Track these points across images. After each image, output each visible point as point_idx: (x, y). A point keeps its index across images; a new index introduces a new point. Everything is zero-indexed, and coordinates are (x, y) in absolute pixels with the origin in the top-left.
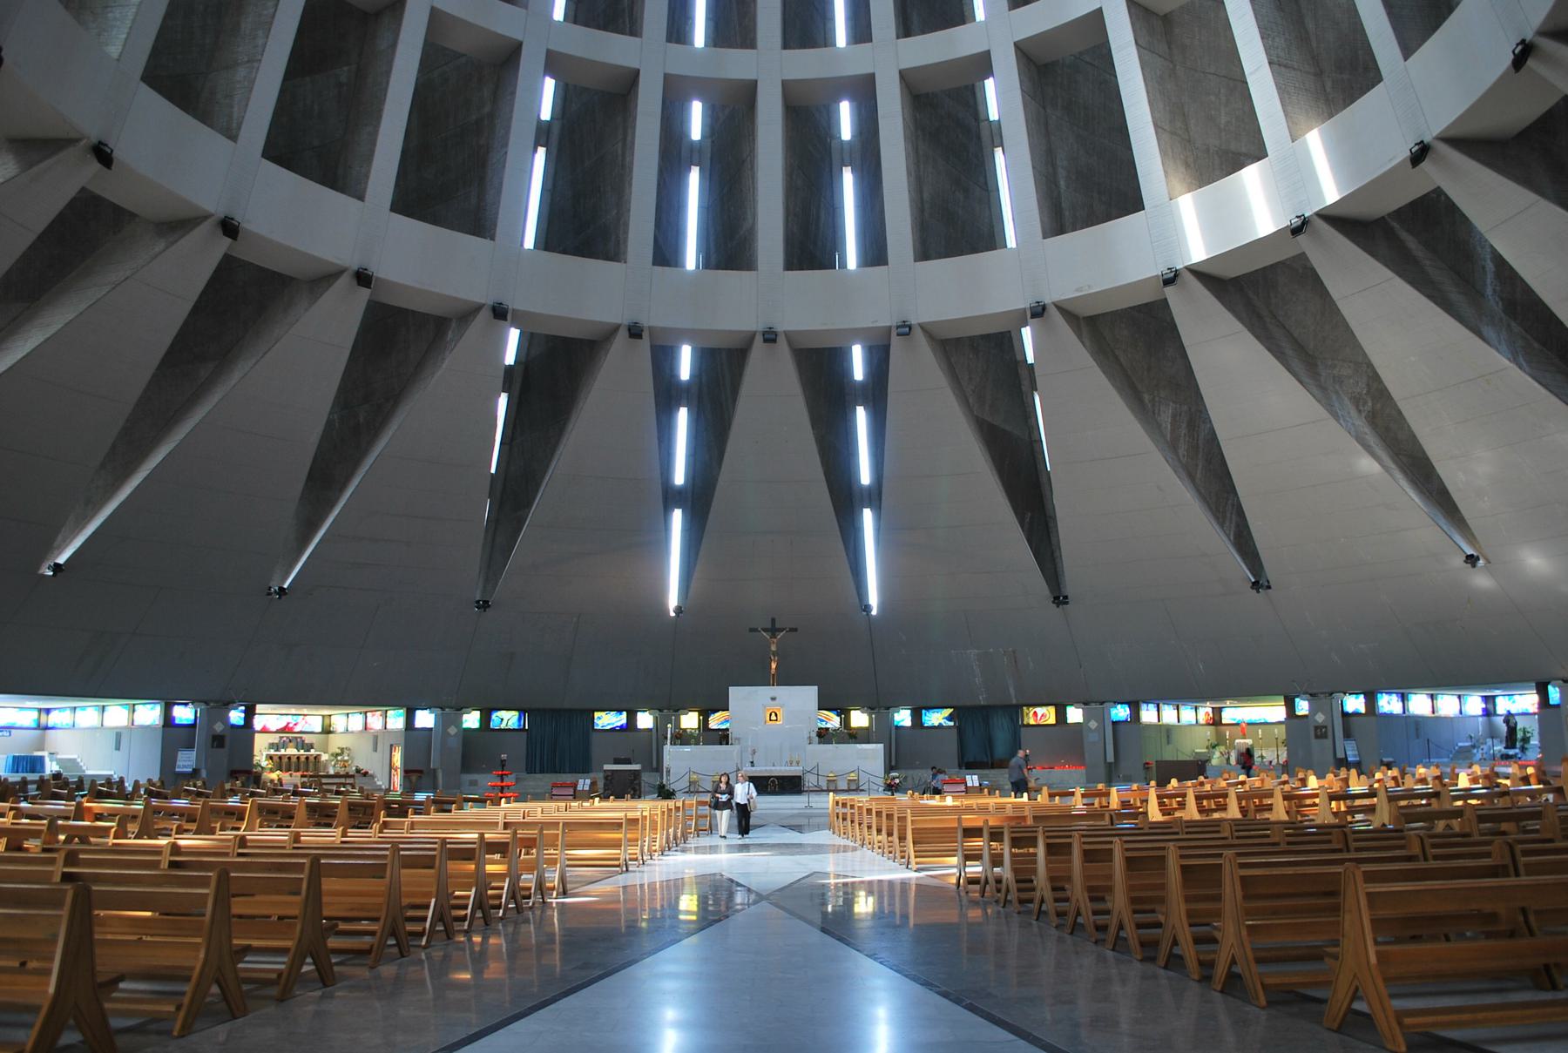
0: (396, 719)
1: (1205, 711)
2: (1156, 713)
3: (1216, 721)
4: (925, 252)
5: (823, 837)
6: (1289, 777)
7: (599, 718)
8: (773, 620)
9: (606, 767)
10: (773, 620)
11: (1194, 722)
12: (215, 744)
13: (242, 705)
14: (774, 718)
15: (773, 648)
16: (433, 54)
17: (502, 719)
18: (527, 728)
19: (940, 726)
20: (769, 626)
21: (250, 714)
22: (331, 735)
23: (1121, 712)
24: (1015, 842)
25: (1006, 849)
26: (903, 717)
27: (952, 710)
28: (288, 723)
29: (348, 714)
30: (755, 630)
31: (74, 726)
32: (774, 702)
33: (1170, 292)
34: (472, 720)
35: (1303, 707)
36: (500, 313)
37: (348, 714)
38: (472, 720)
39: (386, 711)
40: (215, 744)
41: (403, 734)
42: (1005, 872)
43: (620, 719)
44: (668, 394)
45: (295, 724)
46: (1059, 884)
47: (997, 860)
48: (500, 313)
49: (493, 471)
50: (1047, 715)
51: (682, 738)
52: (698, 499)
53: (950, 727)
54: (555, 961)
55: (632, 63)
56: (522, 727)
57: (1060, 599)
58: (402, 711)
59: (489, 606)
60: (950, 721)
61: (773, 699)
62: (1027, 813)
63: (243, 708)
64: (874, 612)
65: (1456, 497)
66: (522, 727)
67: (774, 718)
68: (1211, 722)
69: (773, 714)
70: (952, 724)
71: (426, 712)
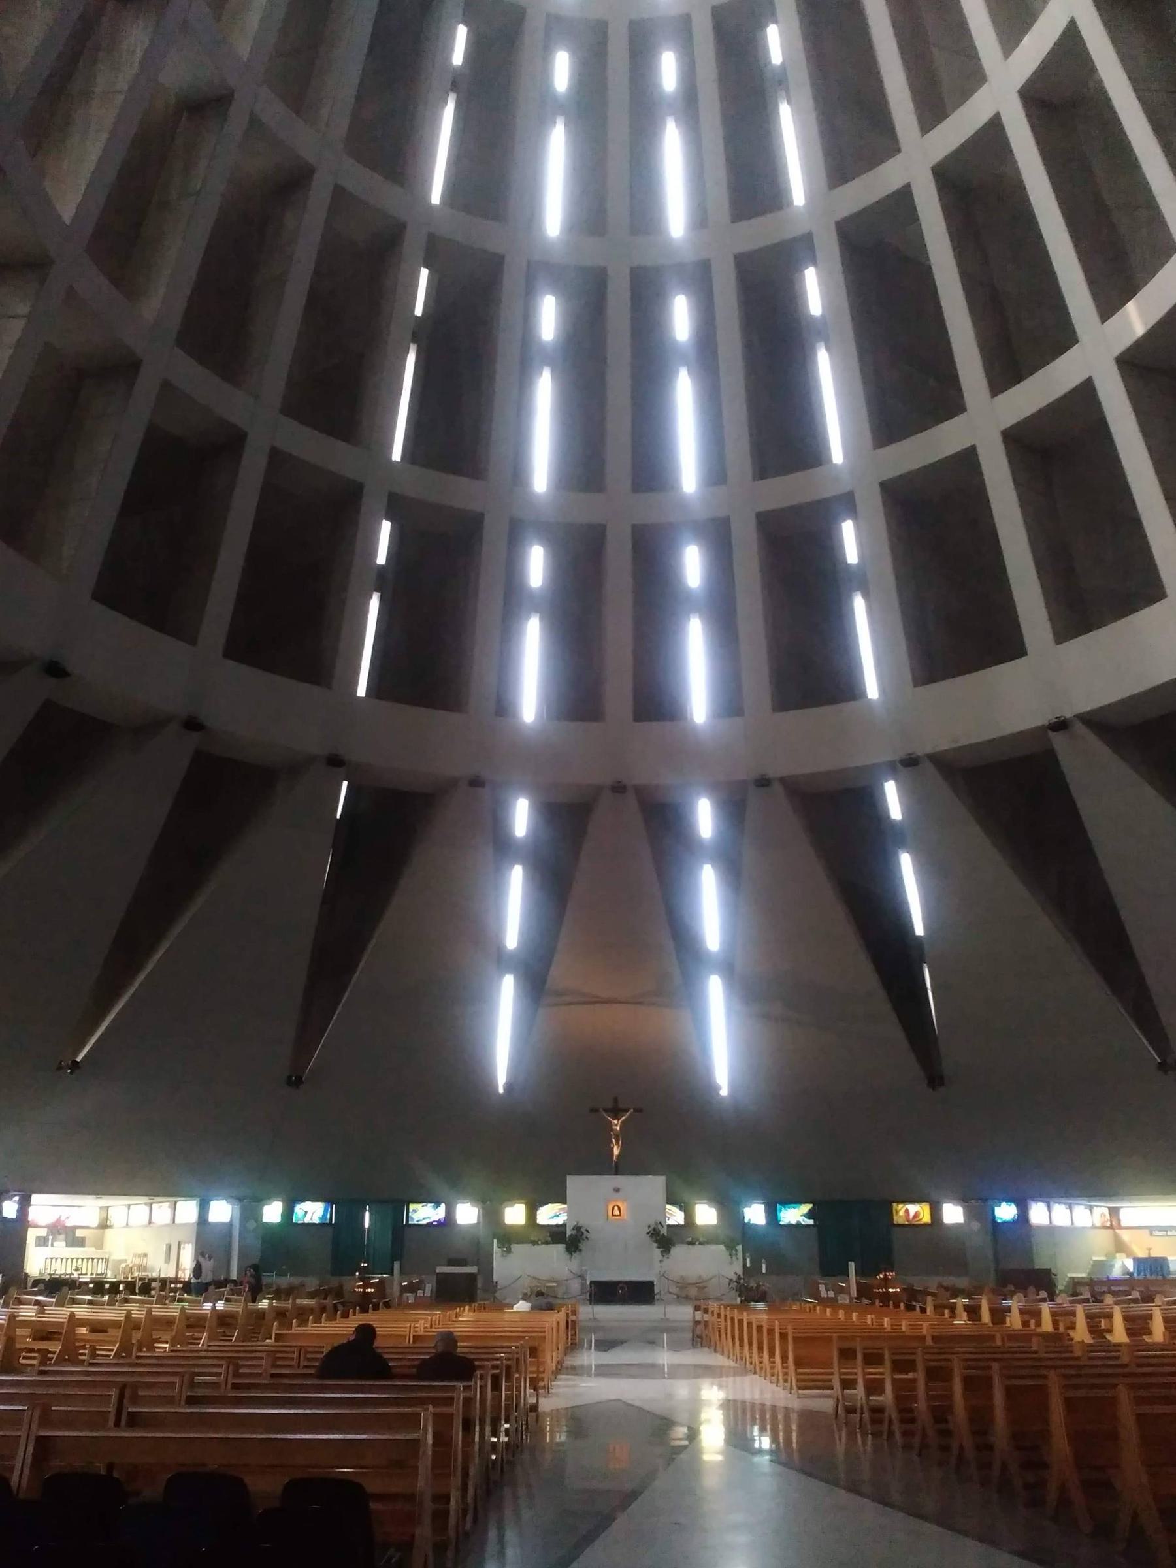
0: (188, 1210)
1: (1100, 1211)
2: (1048, 1213)
5: (665, 1358)
6: (1016, 1288)
7: (415, 1211)
8: (616, 1100)
9: (439, 1270)
10: (616, 1100)
13: (15, 1195)
14: (616, 1212)
16: (270, 492)
17: (306, 1212)
18: (333, 1222)
19: (798, 1225)
20: (610, 1105)
21: (25, 1204)
22: (107, 1231)
23: (1005, 1212)
24: (899, 1367)
25: (885, 1372)
29: (129, 1206)
30: (597, 1110)
31: (127, 1224)
32: (618, 1195)
33: (1058, 741)
34: (272, 1213)
36: (335, 762)
37: (129, 1206)
38: (272, 1213)
39: (176, 1203)
41: (195, 1228)
42: (887, 1398)
45: (68, 1218)
46: (941, 1413)
47: (874, 1387)
48: (335, 762)
51: (509, 1238)
53: (808, 1226)
56: (328, 1221)
57: (935, 1079)
58: (195, 1202)
59: (302, 1082)
60: (809, 1218)
61: (617, 1190)
62: (925, 1332)
65: (1143, 944)
66: (328, 1221)
67: (616, 1212)
68: (1108, 1224)
69: (616, 1208)
70: (811, 1222)
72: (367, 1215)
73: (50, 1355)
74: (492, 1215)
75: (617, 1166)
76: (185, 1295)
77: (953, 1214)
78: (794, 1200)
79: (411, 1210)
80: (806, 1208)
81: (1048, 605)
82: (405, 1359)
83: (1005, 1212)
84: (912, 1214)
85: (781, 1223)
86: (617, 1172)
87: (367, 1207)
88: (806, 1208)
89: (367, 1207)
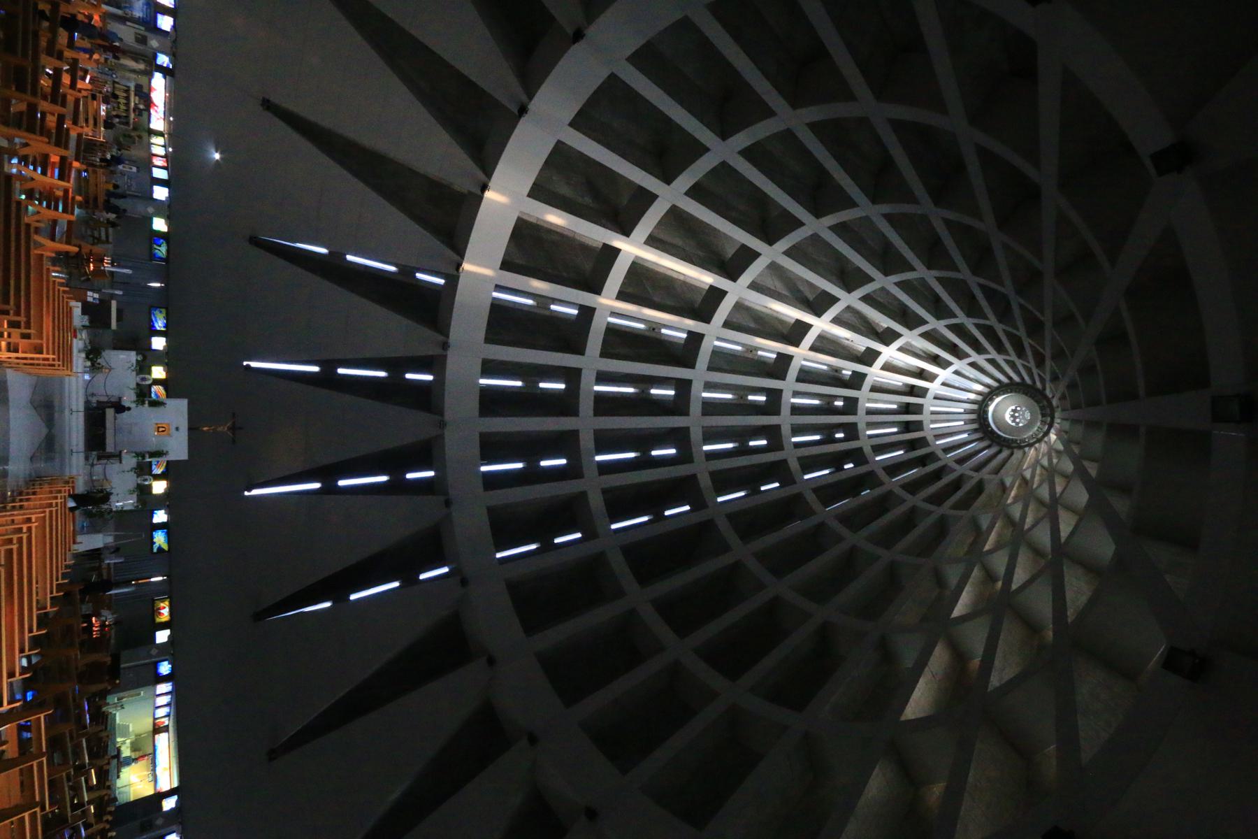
3: (157, 730)
4: (613, 77)
8: (240, 428)
10: (240, 428)
11: (156, 717)
12: (139, 36)
15: (220, 429)
26: (160, 517)
27: (176, 798)
28: (157, 107)
35: (169, 804)
40: (139, 36)
43: (160, 324)
44: (396, 365)
45: (156, 111)
49: (350, 258)
50: (165, 614)
52: (327, 380)
53: (152, 549)
54: (34, 339)
55: (588, 351)
63: (171, 67)
64: (246, 493)
67: (161, 429)
69: (164, 429)
70: (155, 550)
71: (167, 195)
72: (160, 578)
73: (113, 64)
74: (158, 357)
75: (197, 429)
76: (32, 750)
77: (162, 636)
78: (170, 540)
79: (162, 310)
80: (165, 547)
81: (505, 433)
82: (22, 515)
83: (165, 668)
84: (162, 611)
85: (154, 533)
86: (191, 429)
87: (165, 578)
88: (165, 547)
89: (165, 578)
